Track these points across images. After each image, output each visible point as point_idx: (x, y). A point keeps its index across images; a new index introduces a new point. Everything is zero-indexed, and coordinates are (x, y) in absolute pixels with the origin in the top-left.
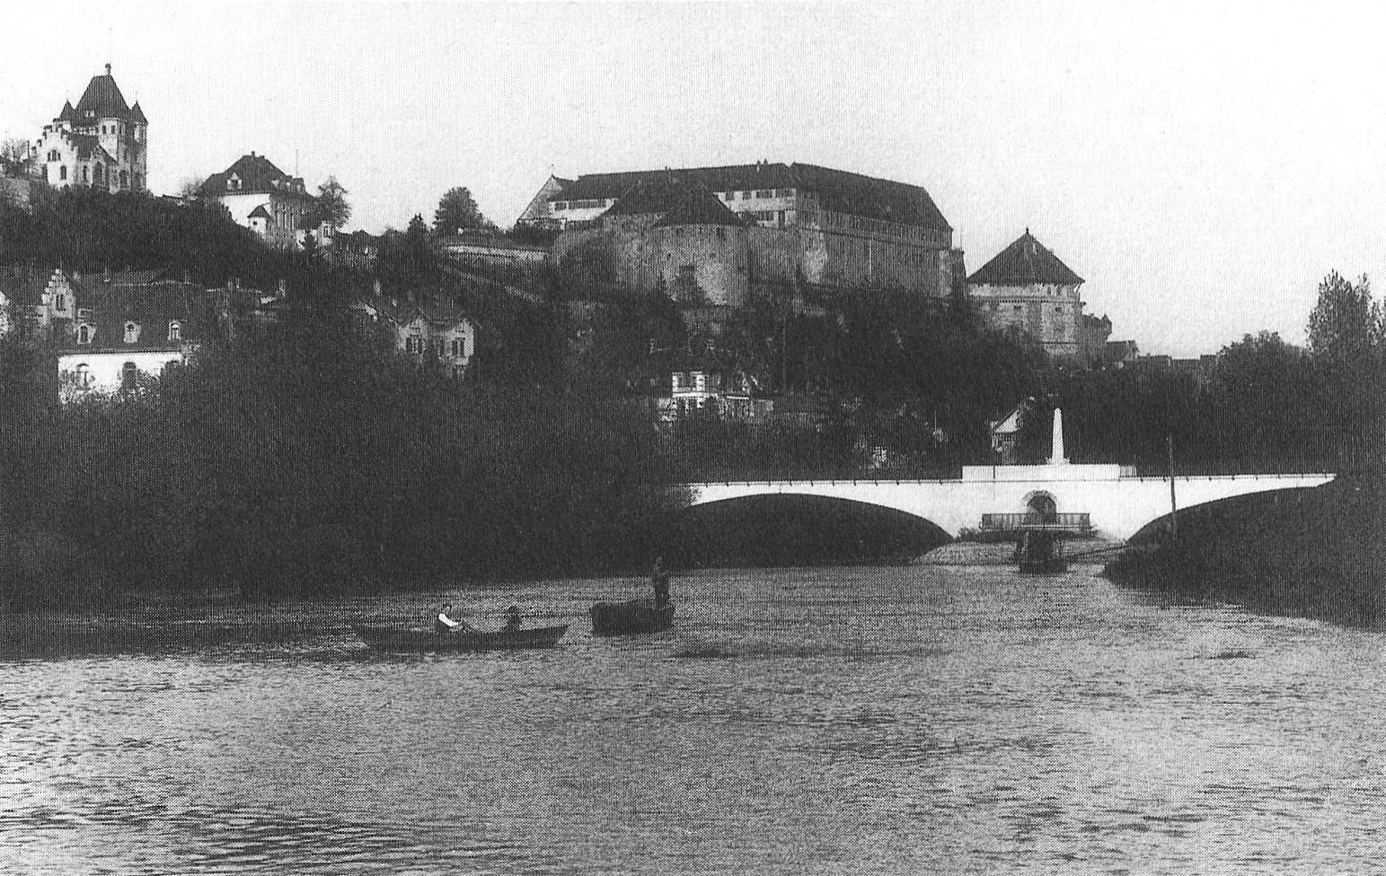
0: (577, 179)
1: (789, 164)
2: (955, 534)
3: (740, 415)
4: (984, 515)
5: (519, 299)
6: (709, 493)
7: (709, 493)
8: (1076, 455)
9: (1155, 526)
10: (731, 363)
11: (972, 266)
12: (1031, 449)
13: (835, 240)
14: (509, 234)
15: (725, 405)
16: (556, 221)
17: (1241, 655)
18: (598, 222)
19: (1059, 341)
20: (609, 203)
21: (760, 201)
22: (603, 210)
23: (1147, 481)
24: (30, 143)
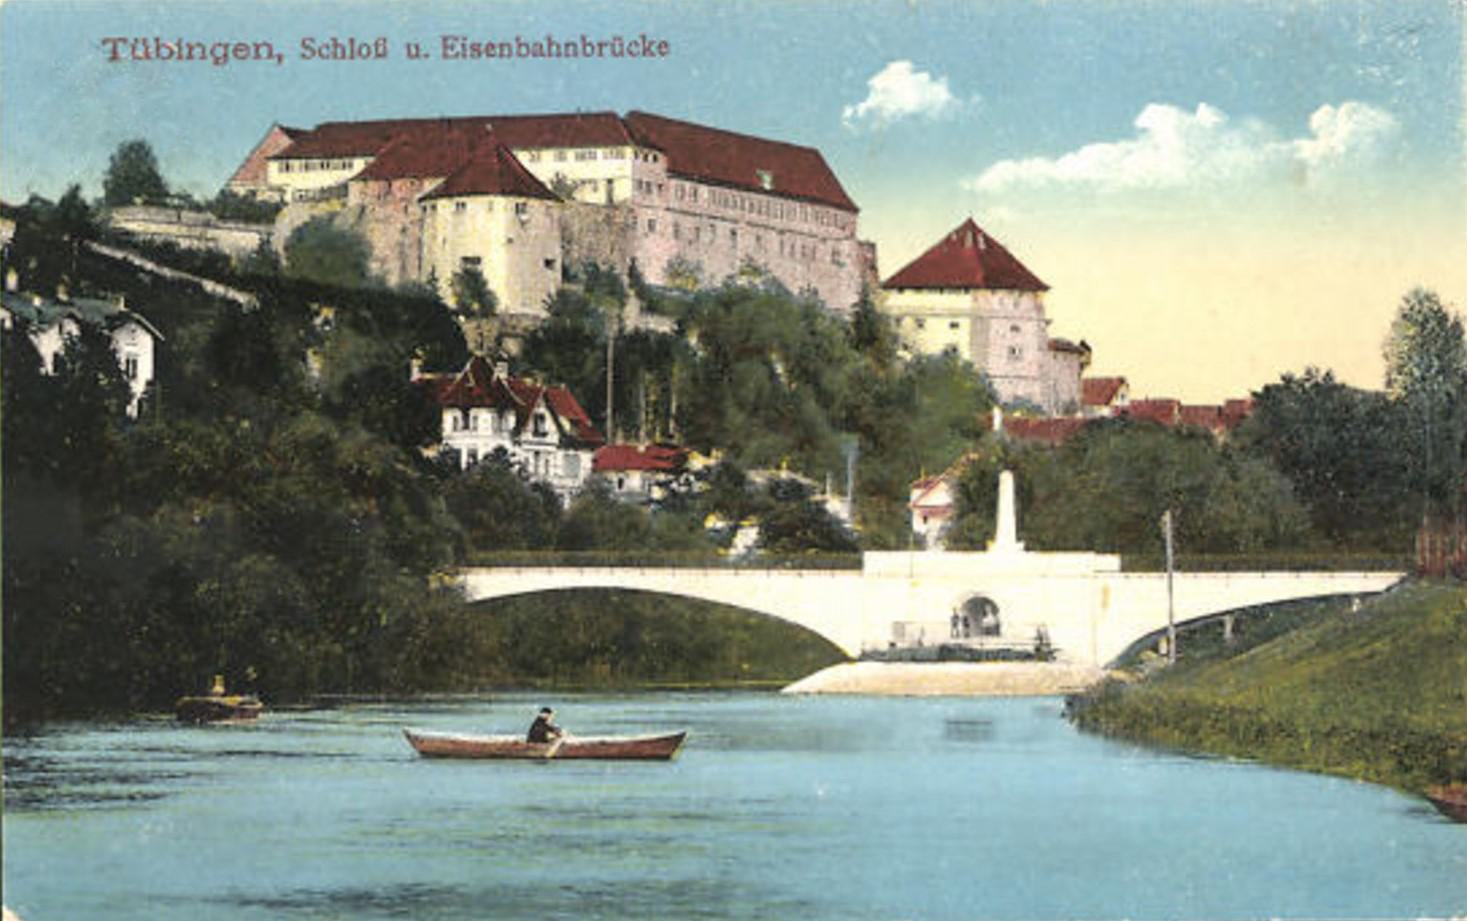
0: (1142, 120)
1: (622, 113)
2: (853, 653)
3: (542, 470)
4: (897, 623)
5: (224, 300)
6: (488, 583)
7: (488, 583)
8: (1037, 536)
9: (804, 636)
10: (532, 395)
11: (887, 269)
12: (970, 530)
13: (687, 223)
14: (210, 206)
15: (520, 454)
16: (281, 190)
17: (675, 817)
18: (342, 190)
19: (1019, 376)
20: (359, 164)
21: (582, 164)
22: (348, 174)
23: (1133, 576)
24: (421, 47)
